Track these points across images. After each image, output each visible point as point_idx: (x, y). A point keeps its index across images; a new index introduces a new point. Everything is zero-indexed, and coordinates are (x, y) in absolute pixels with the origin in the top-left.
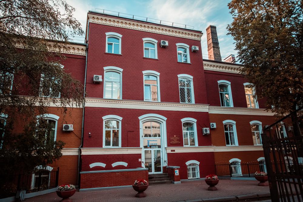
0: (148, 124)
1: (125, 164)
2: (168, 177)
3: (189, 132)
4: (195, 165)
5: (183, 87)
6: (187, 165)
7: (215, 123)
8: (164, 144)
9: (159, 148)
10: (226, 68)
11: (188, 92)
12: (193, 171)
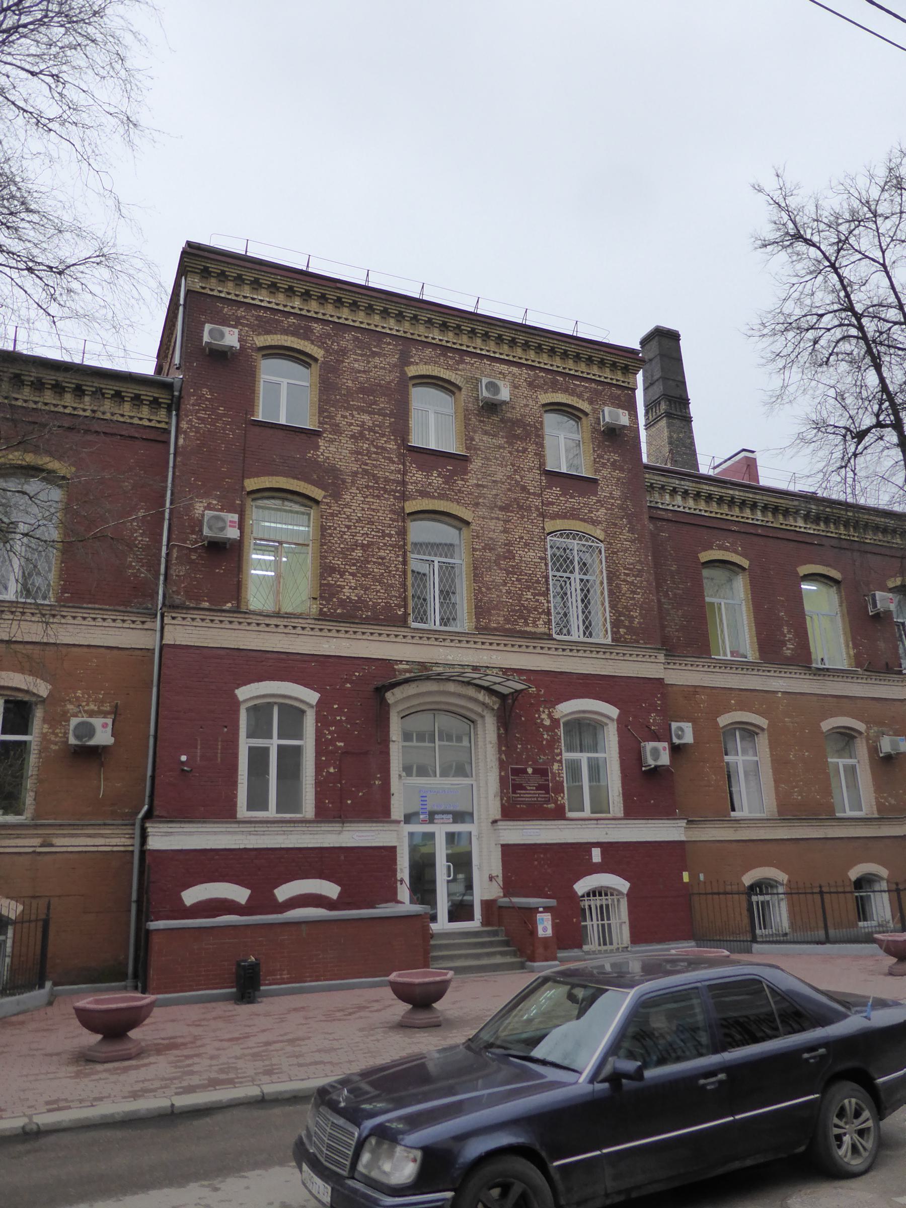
0: (422, 722)
1: (331, 890)
2: (507, 943)
3: (589, 758)
4: (612, 895)
5: (565, 571)
6: (580, 893)
7: (690, 724)
8: (9, 847)
9: (455, 821)
10: (732, 502)
11: (586, 596)
12: (602, 920)
